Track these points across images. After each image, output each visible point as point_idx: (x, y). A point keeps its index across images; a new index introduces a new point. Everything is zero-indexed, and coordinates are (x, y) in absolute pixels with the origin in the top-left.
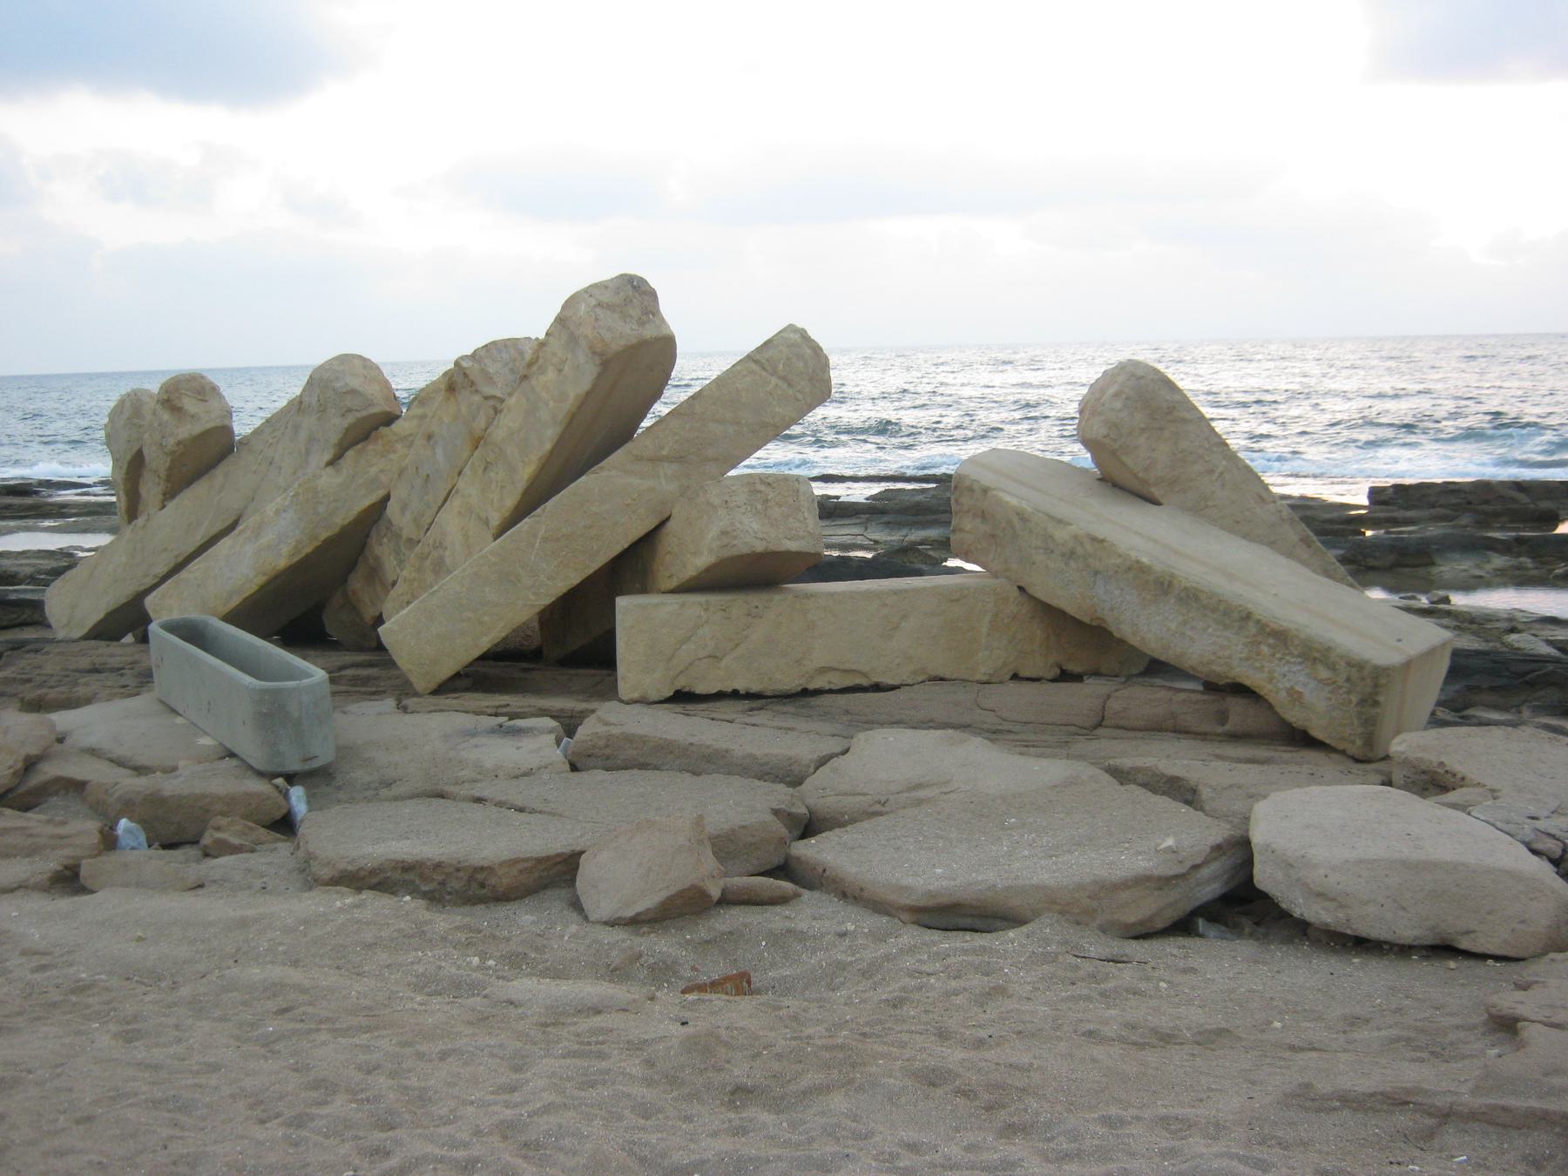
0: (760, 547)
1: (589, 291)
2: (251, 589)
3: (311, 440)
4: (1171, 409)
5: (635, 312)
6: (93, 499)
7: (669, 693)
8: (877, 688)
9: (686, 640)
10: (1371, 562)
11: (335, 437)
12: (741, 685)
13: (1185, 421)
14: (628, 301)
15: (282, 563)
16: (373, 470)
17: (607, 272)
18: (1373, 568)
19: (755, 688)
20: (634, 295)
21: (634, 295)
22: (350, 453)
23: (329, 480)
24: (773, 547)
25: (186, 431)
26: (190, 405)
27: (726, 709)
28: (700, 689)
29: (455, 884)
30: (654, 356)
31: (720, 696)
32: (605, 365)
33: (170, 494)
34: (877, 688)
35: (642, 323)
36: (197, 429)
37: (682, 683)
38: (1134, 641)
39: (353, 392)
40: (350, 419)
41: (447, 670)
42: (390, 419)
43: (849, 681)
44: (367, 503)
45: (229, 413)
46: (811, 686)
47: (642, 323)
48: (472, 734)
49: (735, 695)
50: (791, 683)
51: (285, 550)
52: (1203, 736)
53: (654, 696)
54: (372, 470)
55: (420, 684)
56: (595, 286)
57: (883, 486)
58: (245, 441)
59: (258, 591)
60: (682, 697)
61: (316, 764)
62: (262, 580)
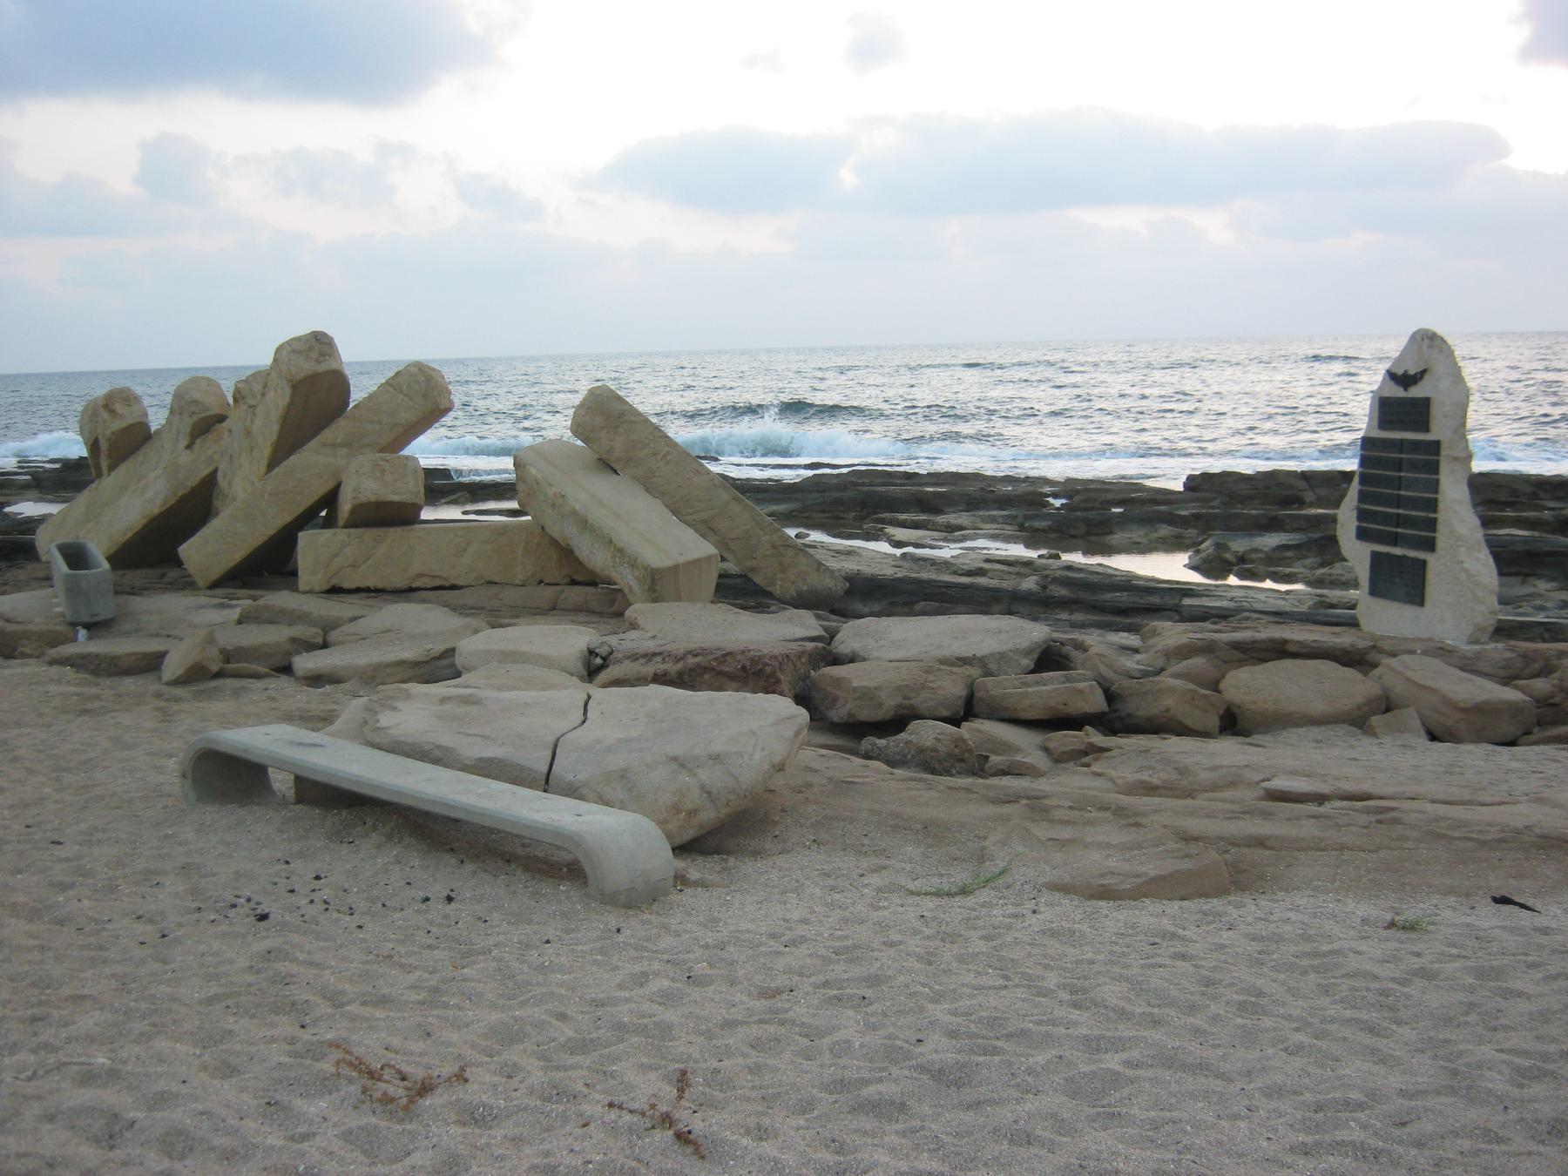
0: (373, 499)
1: (289, 343)
2: (138, 527)
3: (178, 432)
4: (621, 415)
5: (315, 355)
6: (1397, 551)
7: (326, 587)
8: (454, 587)
9: (336, 555)
10: (1072, 531)
11: (188, 430)
12: (371, 583)
13: (632, 422)
14: (310, 349)
15: (156, 511)
16: (210, 452)
17: (303, 329)
18: (1072, 536)
19: (380, 586)
20: (320, 343)
21: (320, 343)
22: (198, 441)
23: (185, 458)
24: (382, 499)
25: (117, 425)
26: (119, 408)
27: (353, 598)
28: (346, 585)
29: (104, 666)
30: (337, 383)
31: (358, 590)
32: (295, 387)
33: (112, 468)
34: (454, 587)
35: (318, 361)
36: (124, 424)
37: (335, 581)
38: (585, 561)
39: (195, 402)
40: (195, 419)
41: (216, 573)
42: (222, 418)
43: (437, 583)
44: (206, 472)
45: (146, 415)
46: (414, 585)
47: (318, 361)
48: (201, 607)
49: (368, 590)
50: (399, 581)
51: (158, 502)
52: (601, 614)
53: (317, 588)
54: (209, 448)
55: (201, 583)
56: (294, 339)
57: (810, 473)
58: (158, 432)
59: (145, 527)
60: (335, 591)
61: (98, 619)
62: (144, 521)
